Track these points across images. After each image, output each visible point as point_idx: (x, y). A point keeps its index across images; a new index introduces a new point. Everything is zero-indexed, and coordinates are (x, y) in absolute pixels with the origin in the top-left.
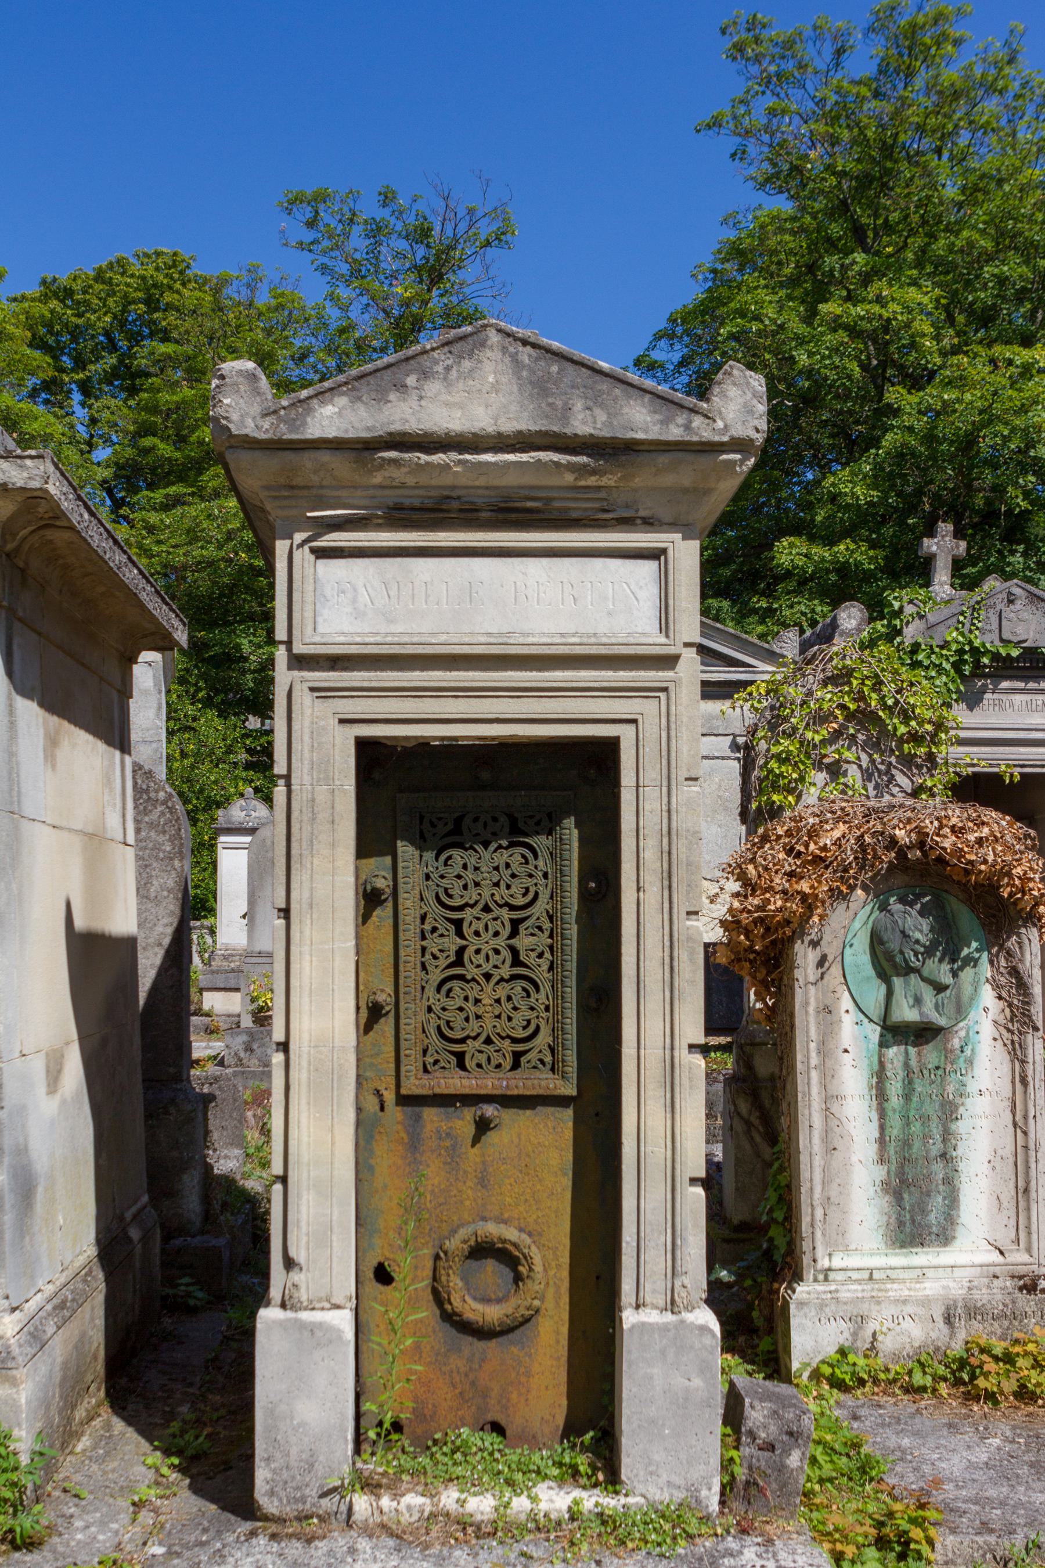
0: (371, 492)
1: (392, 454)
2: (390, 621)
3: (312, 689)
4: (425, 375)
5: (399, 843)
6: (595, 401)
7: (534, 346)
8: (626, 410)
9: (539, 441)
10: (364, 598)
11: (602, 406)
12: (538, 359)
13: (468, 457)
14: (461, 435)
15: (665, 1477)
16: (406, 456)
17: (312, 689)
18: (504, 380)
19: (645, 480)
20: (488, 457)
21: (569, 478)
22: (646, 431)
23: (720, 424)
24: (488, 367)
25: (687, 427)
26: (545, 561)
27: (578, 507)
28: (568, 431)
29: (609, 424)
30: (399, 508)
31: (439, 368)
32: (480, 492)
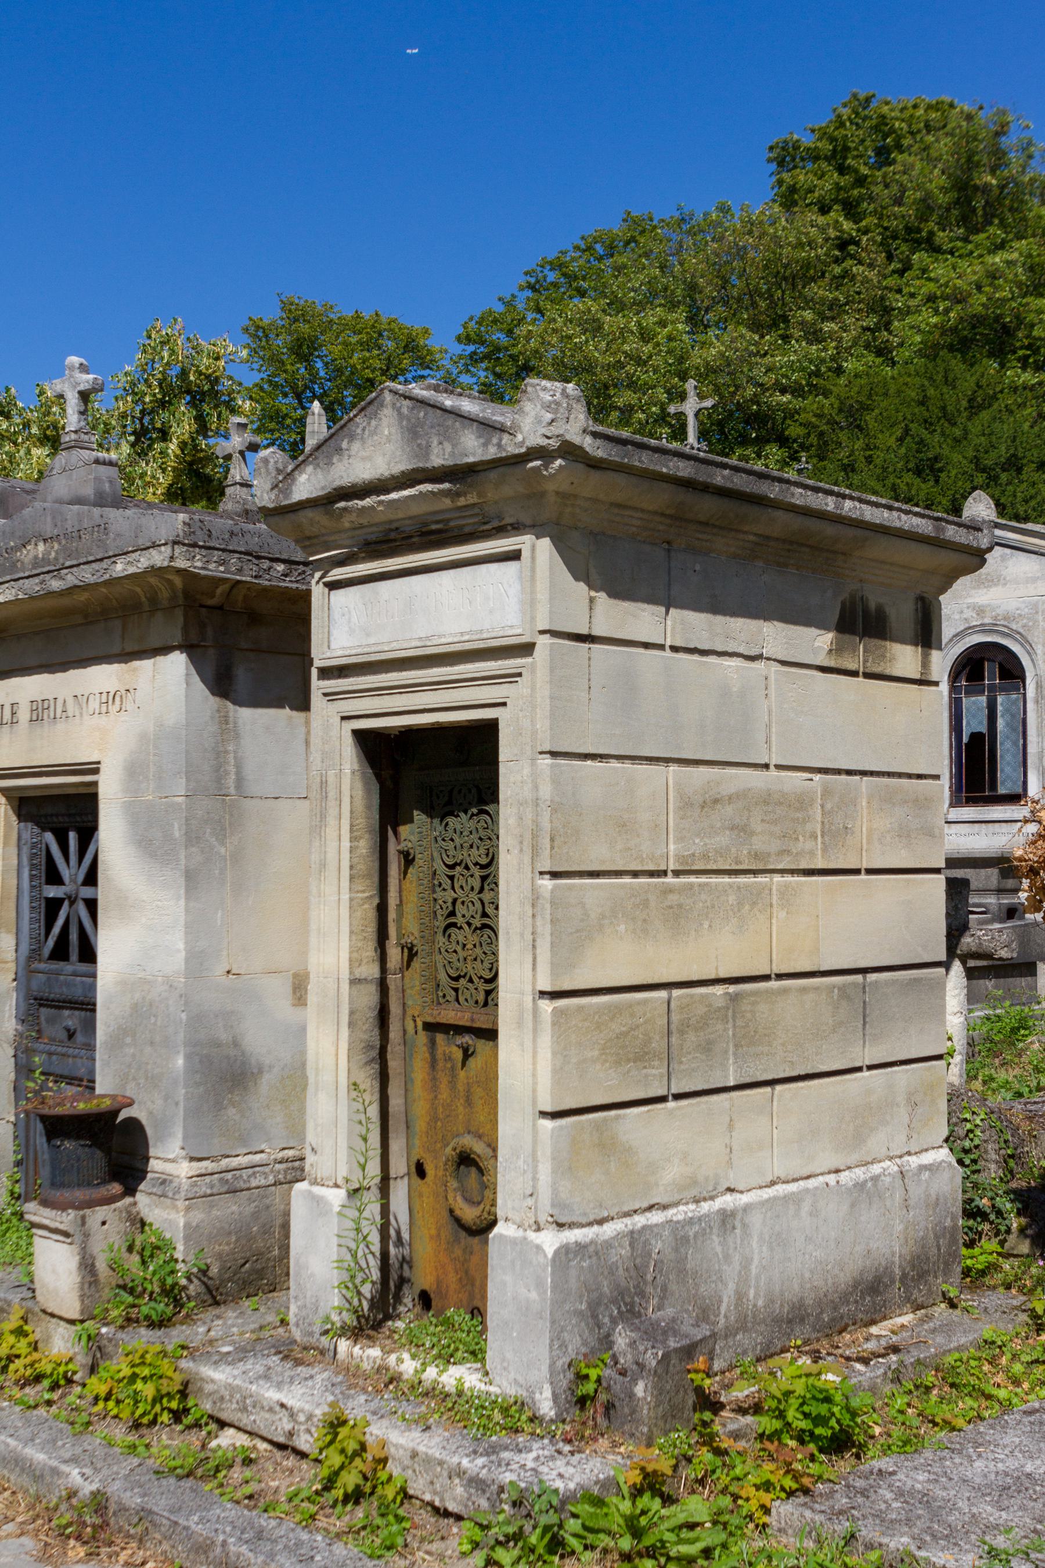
0: (350, 534)
1: (342, 504)
2: (368, 635)
3: (325, 695)
4: (352, 438)
5: (415, 813)
6: (446, 436)
7: (410, 398)
8: (463, 439)
9: (420, 477)
10: (354, 619)
11: (448, 439)
12: (413, 408)
13: (382, 498)
14: (371, 482)
15: (512, 1376)
16: (350, 504)
17: (325, 695)
18: (393, 431)
19: (497, 492)
20: (394, 496)
21: (447, 502)
22: (474, 455)
23: (520, 437)
24: (385, 422)
25: (499, 445)
26: (452, 572)
27: (469, 523)
28: (429, 465)
29: (452, 454)
30: (367, 544)
31: (359, 431)
32: (407, 522)
